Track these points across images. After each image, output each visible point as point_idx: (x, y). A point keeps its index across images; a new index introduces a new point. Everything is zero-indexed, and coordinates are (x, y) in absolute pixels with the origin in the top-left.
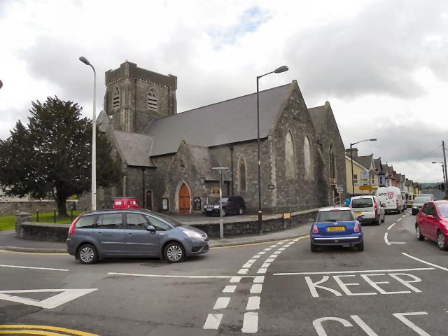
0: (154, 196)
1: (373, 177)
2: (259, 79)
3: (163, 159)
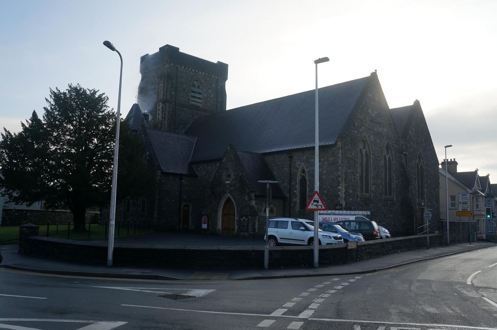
1: (477, 200)
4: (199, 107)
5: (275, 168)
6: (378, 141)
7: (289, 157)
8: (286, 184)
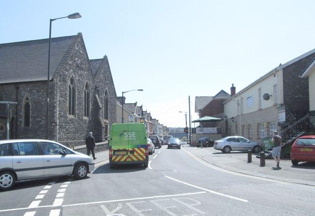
5: (5, 96)
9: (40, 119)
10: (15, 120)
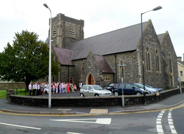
0: (74, 80)
2: (142, 15)
3: (78, 61)
4: (73, 38)
6: (153, 48)
7: (115, 56)
8: (114, 68)
9: (129, 74)
10: (115, 74)
